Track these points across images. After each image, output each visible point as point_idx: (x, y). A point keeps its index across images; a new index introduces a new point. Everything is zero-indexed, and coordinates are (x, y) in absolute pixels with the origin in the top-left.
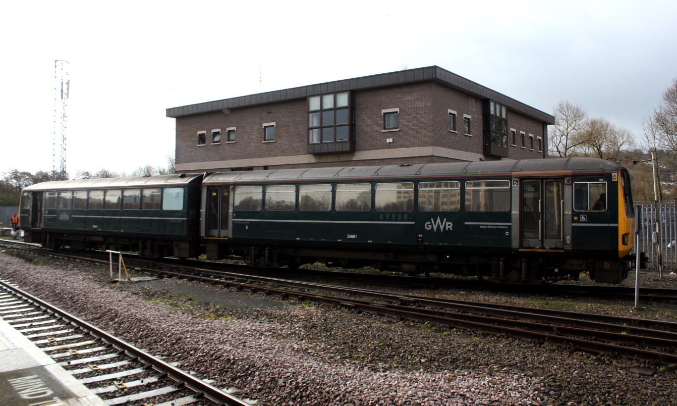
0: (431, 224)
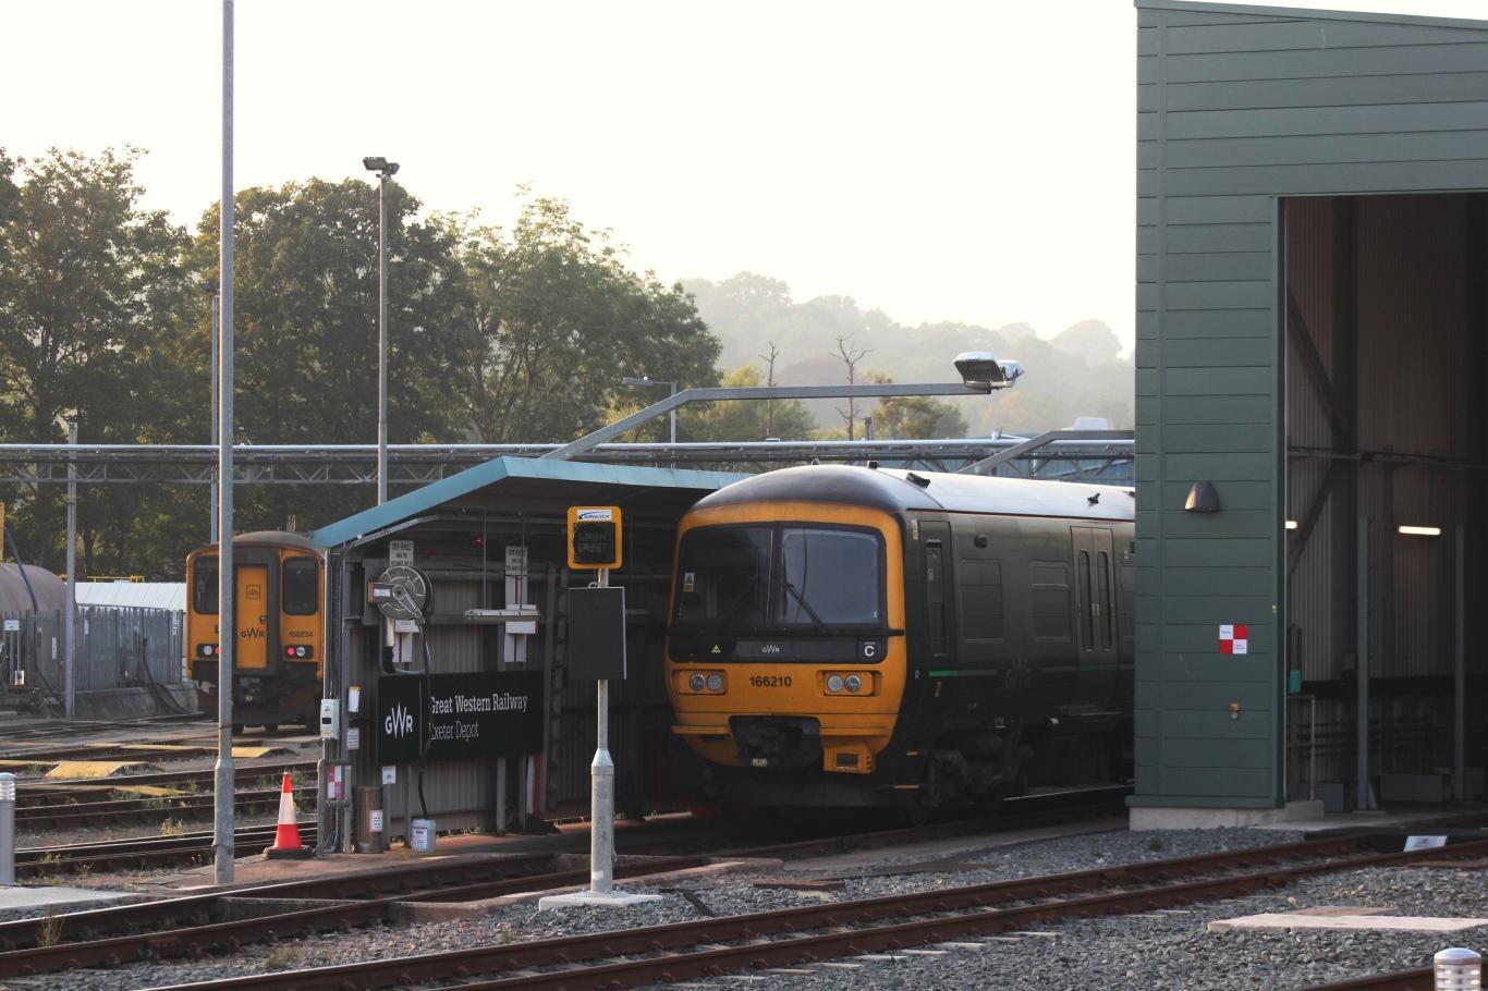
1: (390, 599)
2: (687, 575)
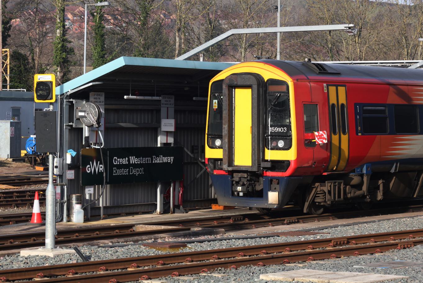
0: (90, 167)
1: (85, 117)
2: (214, 101)
